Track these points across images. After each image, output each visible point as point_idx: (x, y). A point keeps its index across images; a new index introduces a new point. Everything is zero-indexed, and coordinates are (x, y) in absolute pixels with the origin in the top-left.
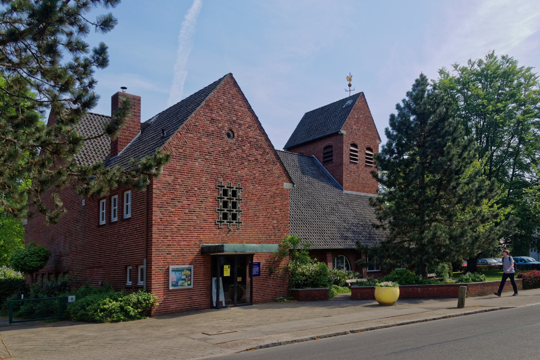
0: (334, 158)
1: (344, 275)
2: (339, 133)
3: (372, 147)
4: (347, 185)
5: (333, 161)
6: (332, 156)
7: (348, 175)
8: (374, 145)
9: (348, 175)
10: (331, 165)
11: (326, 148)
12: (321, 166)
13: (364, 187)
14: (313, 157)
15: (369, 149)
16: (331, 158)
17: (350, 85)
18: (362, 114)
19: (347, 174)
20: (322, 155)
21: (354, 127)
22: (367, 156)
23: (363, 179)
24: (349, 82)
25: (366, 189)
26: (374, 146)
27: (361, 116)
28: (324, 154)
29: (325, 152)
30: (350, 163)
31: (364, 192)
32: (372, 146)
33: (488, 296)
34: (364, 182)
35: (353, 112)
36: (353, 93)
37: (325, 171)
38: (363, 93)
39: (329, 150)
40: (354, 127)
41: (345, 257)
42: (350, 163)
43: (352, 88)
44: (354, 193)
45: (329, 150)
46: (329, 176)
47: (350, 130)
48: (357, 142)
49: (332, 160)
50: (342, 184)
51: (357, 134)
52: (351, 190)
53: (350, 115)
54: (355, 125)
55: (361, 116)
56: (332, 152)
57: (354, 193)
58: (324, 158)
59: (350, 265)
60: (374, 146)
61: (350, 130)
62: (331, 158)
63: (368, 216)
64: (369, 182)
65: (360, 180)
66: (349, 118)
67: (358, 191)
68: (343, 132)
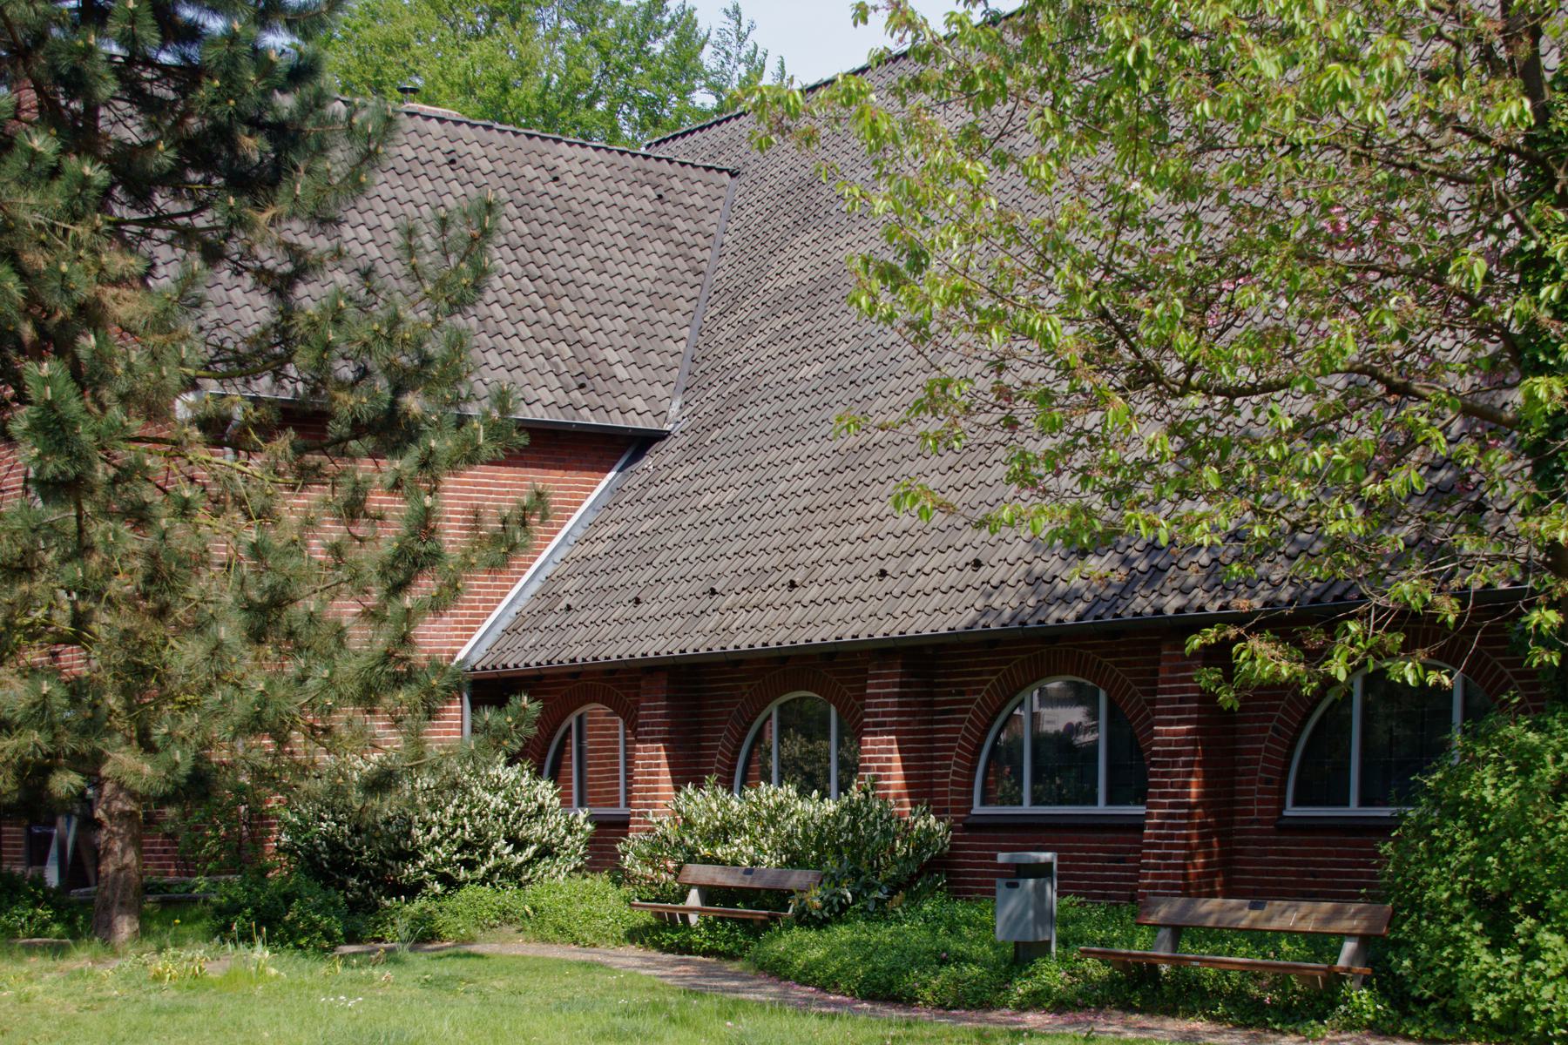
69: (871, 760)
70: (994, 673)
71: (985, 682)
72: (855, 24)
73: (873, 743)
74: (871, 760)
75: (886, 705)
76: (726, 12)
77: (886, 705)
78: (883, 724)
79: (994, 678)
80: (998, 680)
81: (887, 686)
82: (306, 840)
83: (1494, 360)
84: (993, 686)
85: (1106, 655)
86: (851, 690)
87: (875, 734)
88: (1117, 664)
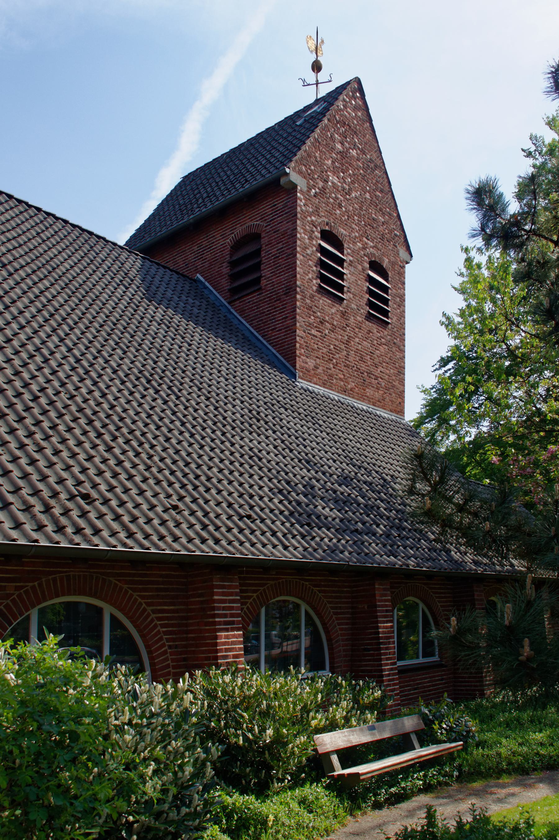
0: (266, 272)
1: (306, 710)
2: (283, 181)
3: (385, 263)
4: (311, 363)
5: (263, 282)
6: (257, 267)
7: (313, 332)
8: (392, 259)
9: (313, 332)
10: (254, 298)
11: (237, 245)
12: (223, 305)
13: (364, 385)
14: (197, 281)
15: (376, 266)
16: (255, 276)
17: (317, 67)
18: (355, 147)
19: (310, 325)
20: (225, 270)
21: (332, 178)
22: (372, 274)
23: (362, 359)
24: (313, 58)
25: (369, 392)
26: (393, 264)
27: (354, 153)
28: (233, 264)
29: (234, 258)
30: (318, 291)
31: (362, 398)
32: (386, 260)
33: (446, 752)
34: (363, 367)
35: (326, 127)
36: (325, 90)
37: (235, 322)
38: (358, 81)
39: (250, 249)
40: (332, 178)
41: (304, 607)
42: (318, 291)
43: (323, 76)
44: (335, 395)
45: (250, 249)
46: (247, 334)
47: (321, 184)
48: (342, 231)
49: (257, 281)
50: (291, 357)
51: (340, 206)
52: (324, 385)
53: (318, 131)
54: (334, 173)
55: (354, 153)
56: (257, 253)
57: (335, 395)
58: (233, 277)
59: (329, 640)
60: (393, 264)
61: (321, 184)
62: (255, 276)
63: (383, 464)
64: (377, 372)
65: (351, 359)
66: (316, 140)
67: (344, 391)
68: (295, 177)
69: (227, 650)
70: (255, 591)
71: (249, 598)
72: (444, 315)
73: (227, 637)
74: (227, 650)
75: (232, 608)
76: (462, 247)
77: (232, 608)
78: (232, 623)
79: (255, 595)
80: (258, 596)
81: (231, 594)
82: (221, 665)
83: (436, 702)
84: (254, 600)
85: (315, 586)
86: (143, 597)
87: (227, 630)
88: (319, 591)
